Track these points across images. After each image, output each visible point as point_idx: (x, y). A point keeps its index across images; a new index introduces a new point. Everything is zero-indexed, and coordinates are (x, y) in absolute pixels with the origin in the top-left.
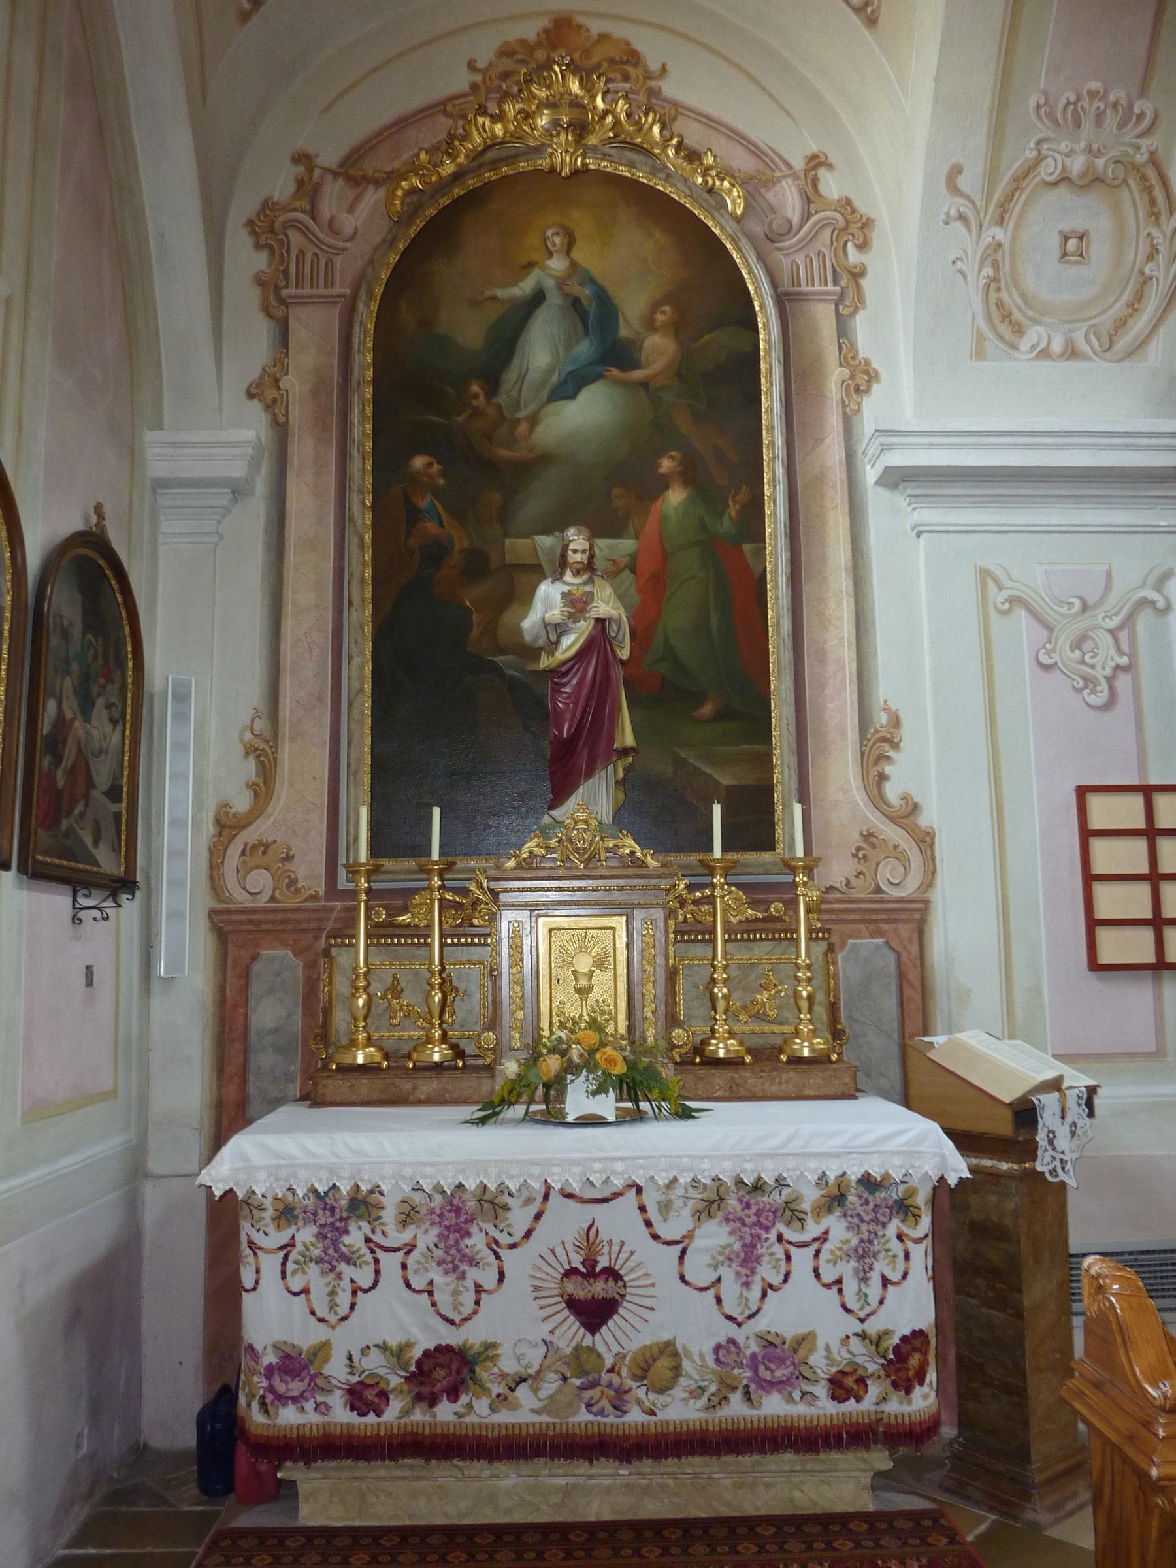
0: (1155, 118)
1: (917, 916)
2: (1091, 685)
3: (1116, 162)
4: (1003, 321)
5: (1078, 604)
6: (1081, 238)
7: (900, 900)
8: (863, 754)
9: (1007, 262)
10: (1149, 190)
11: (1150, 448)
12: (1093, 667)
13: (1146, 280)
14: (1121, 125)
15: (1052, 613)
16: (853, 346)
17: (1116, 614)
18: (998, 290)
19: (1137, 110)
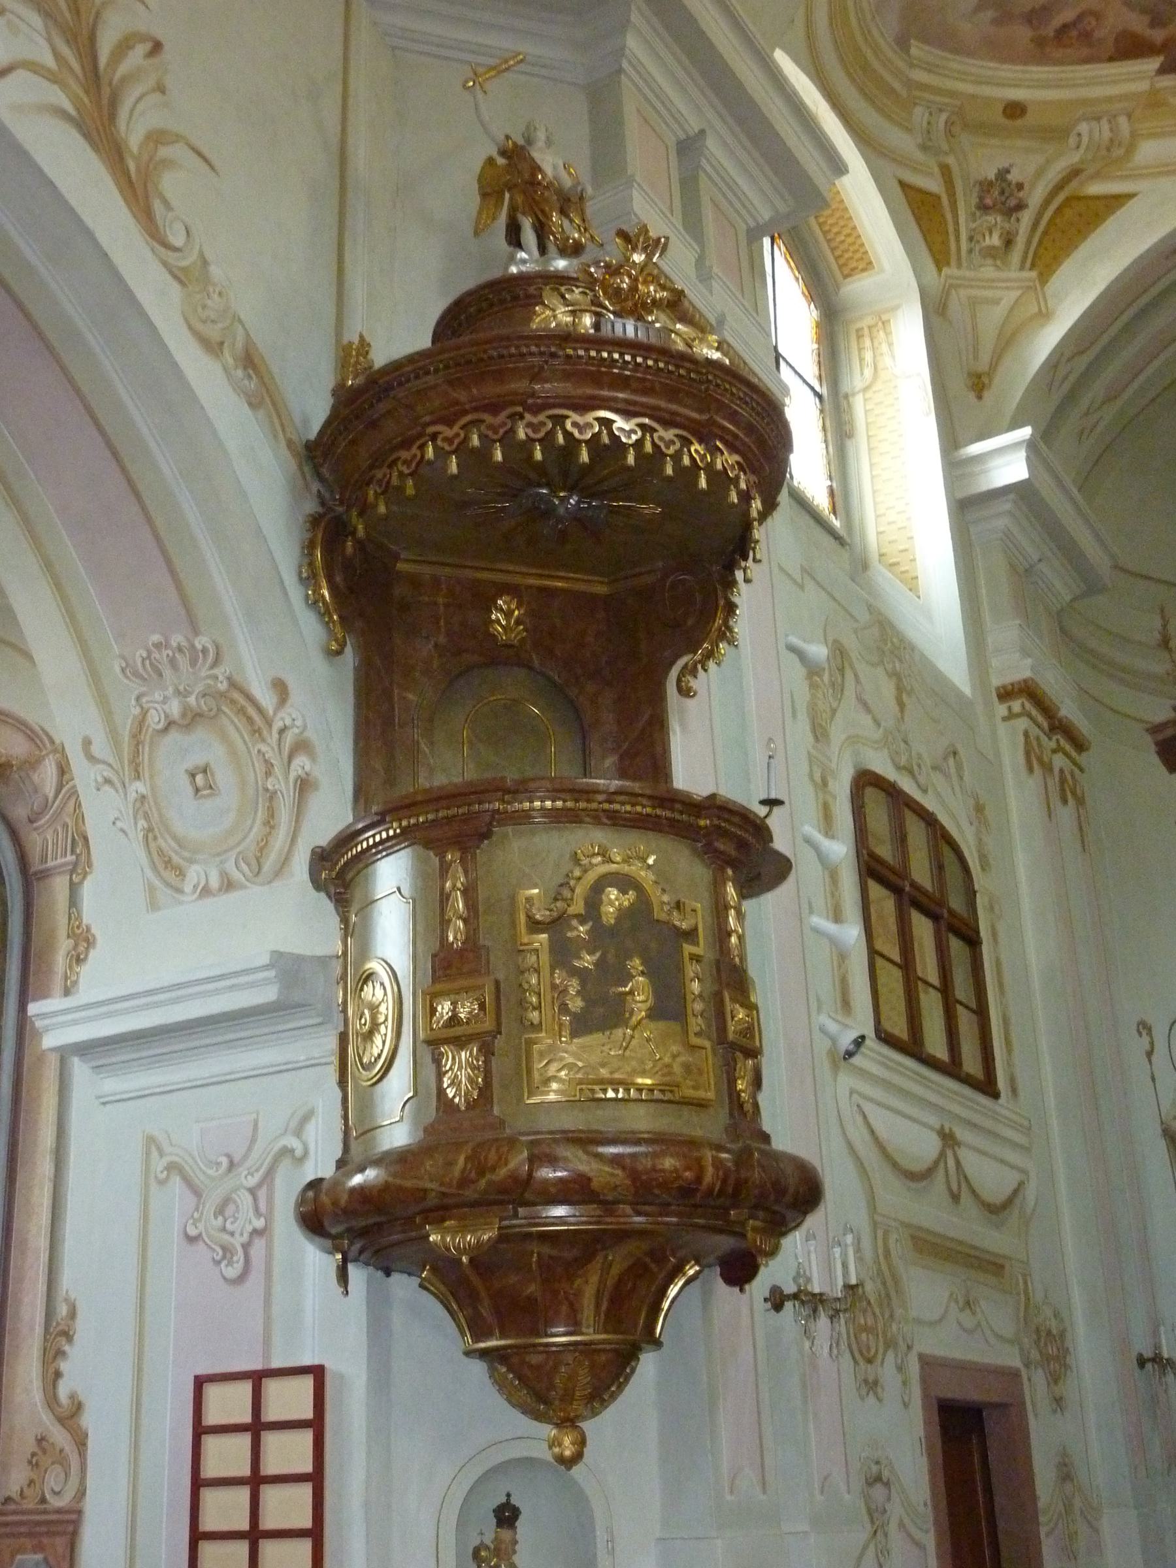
0: (217, 647)
1: (71, 1528)
2: (228, 1255)
3: (204, 695)
4: (166, 868)
5: (225, 1161)
6: (205, 771)
7: (59, 1511)
8: (45, 1350)
9: (154, 809)
10: (242, 711)
11: (252, 985)
12: (232, 1234)
13: (272, 796)
14: (193, 662)
15: (202, 1177)
16: (79, 917)
17: (257, 1170)
18: (155, 838)
19: (199, 647)
